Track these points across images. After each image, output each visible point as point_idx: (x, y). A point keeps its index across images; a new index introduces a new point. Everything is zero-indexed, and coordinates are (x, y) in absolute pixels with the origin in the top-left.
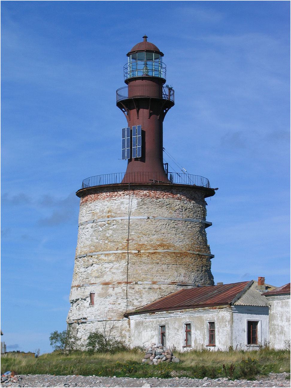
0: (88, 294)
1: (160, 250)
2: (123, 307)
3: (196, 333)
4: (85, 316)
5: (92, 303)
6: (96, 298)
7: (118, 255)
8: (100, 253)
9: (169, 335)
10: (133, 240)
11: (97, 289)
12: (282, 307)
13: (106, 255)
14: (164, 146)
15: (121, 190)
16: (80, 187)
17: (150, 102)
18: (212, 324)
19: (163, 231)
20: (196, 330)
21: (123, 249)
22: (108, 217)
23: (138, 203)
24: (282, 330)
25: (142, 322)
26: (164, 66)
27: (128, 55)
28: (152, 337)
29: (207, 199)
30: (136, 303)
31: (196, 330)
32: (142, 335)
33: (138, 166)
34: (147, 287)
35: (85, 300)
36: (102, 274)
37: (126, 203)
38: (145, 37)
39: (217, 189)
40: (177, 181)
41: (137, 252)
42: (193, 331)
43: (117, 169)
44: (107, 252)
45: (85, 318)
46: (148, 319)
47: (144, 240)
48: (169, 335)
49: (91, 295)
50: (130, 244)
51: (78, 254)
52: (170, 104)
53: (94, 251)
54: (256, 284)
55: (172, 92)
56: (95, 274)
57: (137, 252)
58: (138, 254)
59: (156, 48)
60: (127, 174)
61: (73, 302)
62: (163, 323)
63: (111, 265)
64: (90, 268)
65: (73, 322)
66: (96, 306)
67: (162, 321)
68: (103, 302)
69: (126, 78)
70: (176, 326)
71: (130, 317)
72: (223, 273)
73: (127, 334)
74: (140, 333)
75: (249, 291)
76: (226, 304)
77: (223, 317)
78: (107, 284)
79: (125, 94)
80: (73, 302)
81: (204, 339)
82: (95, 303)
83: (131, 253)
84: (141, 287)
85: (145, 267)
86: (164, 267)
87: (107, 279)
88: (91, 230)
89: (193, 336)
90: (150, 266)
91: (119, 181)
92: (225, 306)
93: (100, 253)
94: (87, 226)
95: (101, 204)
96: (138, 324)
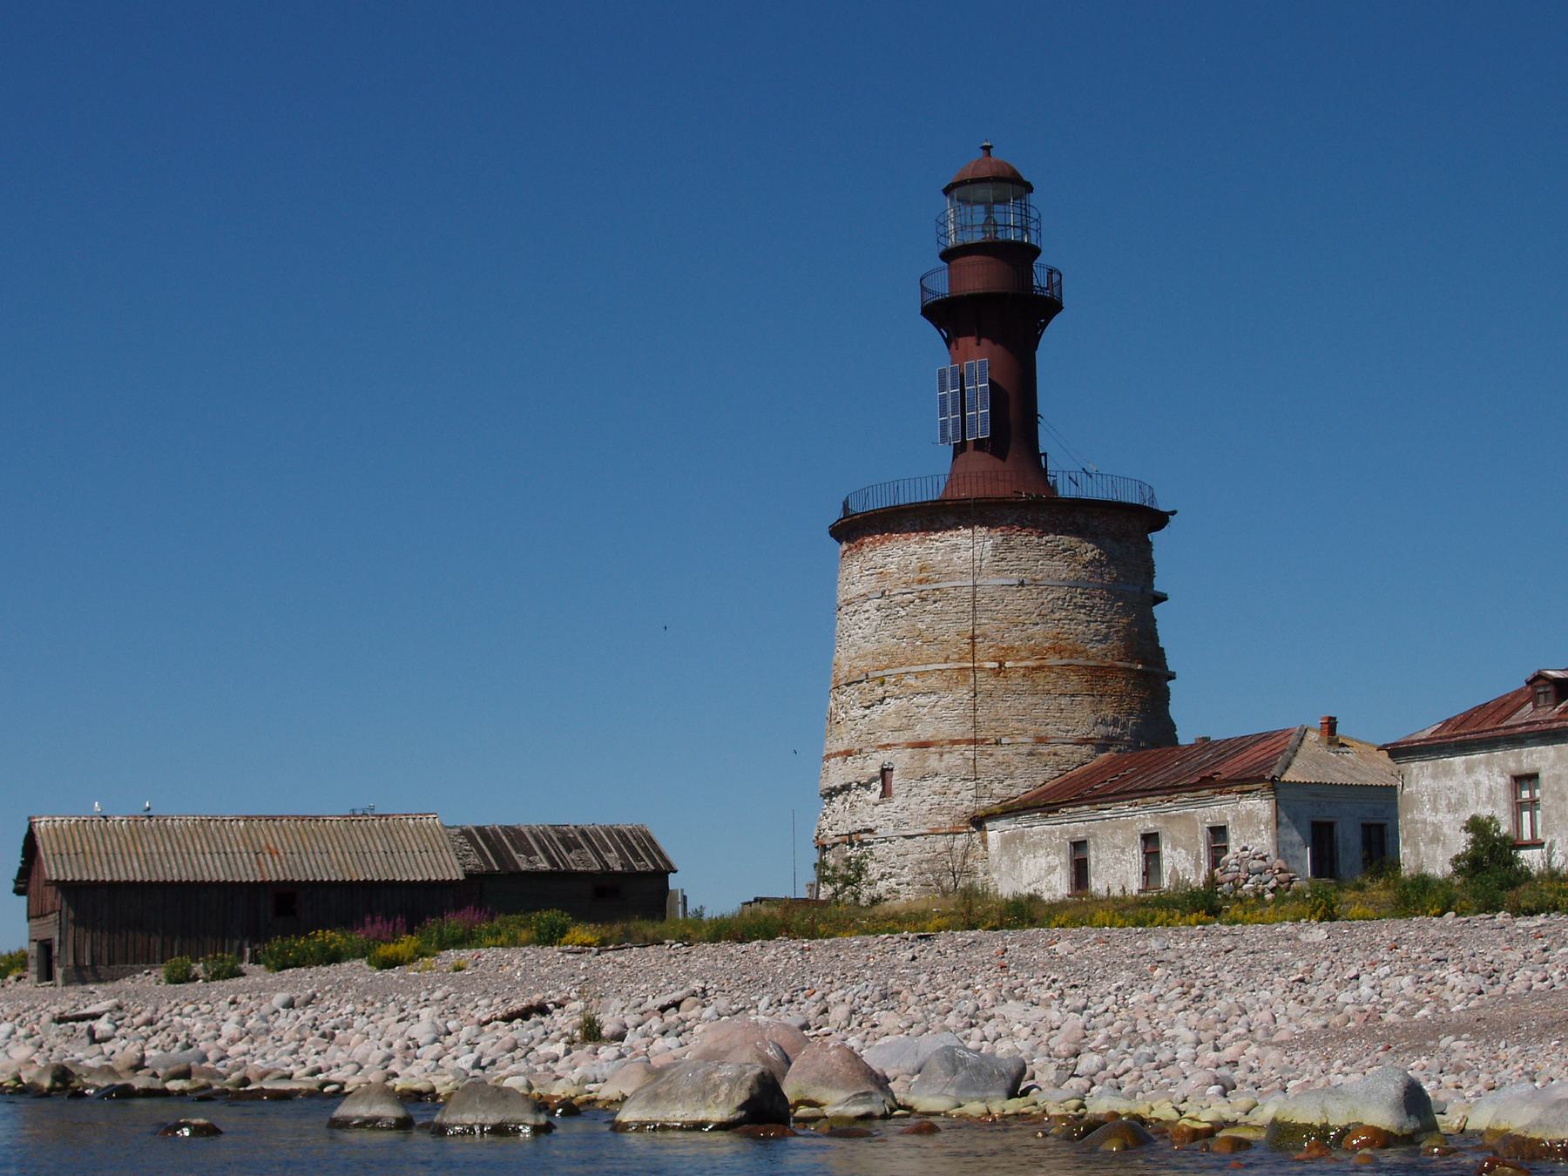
0: (875, 770)
1: (1053, 660)
2: (966, 799)
3: (1175, 854)
4: (871, 825)
5: (886, 793)
6: (896, 779)
7: (948, 673)
8: (903, 670)
9: (1097, 863)
10: (985, 636)
11: (900, 760)
12: (1434, 777)
13: (917, 675)
14: (1042, 407)
15: (951, 520)
16: (836, 515)
17: (999, 308)
18: (1079, 846)
19: (1057, 616)
20: (1174, 848)
21: (961, 659)
22: (920, 582)
23: (996, 547)
24: (1435, 831)
25: (1022, 837)
26: (1034, 214)
27: (947, 191)
28: (1051, 870)
29: (1154, 537)
30: (997, 788)
31: (1174, 848)
32: (1029, 864)
33: (979, 462)
34: (1025, 749)
35: (867, 786)
36: (909, 722)
37: (964, 550)
38: (987, 149)
39: (1173, 513)
40: (1065, 490)
41: (996, 665)
42: (1166, 850)
43: (927, 470)
44: (923, 668)
45: (870, 831)
46: (1038, 827)
47: (1013, 638)
48: (1097, 863)
49: (885, 773)
50: (979, 646)
51: (841, 675)
52: (1052, 307)
53: (887, 667)
54: (1313, 736)
55: (1055, 278)
56: (893, 722)
57: (996, 665)
58: (1000, 671)
59: (1015, 173)
60: (953, 478)
61: (831, 793)
62: (1081, 836)
63: (934, 698)
64: (878, 708)
65: (837, 840)
66: (898, 801)
67: (1077, 829)
68: (915, 790)
69: (942, 248)
70: (1119, 839)
71: (988, 825)
72: (1195, 715)
73: (980, 866)
74: (1015, 862)
75: (1302, 750)
76: (1261, 779)
77: (1250, 813)
78: (925, 745)
79: (941, 287)
80: (831, 793)
81: (1197, 865)
82: (895, 792)
83: (982, 669)
84: (1009, 750)
85: (1021, 704)
86: (1064, 701)
87: (924, 732)
88: (873, 614)
89: (1166, 865)
90: (1030, 700)
91: (930, 492)
92: (1255, 786)
93: (903, 670)
94: (866, 606)
95: (900, 554)
96: (1007, 842)
